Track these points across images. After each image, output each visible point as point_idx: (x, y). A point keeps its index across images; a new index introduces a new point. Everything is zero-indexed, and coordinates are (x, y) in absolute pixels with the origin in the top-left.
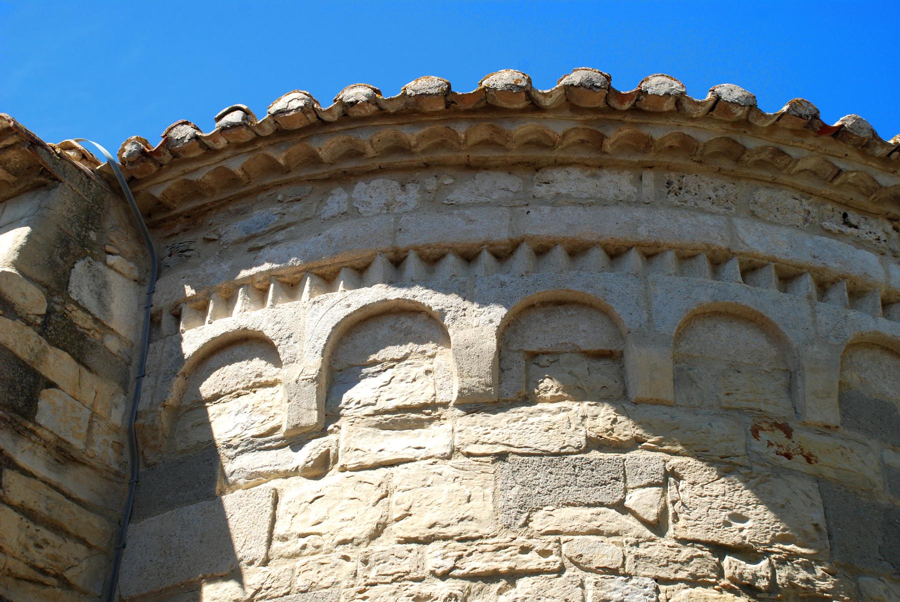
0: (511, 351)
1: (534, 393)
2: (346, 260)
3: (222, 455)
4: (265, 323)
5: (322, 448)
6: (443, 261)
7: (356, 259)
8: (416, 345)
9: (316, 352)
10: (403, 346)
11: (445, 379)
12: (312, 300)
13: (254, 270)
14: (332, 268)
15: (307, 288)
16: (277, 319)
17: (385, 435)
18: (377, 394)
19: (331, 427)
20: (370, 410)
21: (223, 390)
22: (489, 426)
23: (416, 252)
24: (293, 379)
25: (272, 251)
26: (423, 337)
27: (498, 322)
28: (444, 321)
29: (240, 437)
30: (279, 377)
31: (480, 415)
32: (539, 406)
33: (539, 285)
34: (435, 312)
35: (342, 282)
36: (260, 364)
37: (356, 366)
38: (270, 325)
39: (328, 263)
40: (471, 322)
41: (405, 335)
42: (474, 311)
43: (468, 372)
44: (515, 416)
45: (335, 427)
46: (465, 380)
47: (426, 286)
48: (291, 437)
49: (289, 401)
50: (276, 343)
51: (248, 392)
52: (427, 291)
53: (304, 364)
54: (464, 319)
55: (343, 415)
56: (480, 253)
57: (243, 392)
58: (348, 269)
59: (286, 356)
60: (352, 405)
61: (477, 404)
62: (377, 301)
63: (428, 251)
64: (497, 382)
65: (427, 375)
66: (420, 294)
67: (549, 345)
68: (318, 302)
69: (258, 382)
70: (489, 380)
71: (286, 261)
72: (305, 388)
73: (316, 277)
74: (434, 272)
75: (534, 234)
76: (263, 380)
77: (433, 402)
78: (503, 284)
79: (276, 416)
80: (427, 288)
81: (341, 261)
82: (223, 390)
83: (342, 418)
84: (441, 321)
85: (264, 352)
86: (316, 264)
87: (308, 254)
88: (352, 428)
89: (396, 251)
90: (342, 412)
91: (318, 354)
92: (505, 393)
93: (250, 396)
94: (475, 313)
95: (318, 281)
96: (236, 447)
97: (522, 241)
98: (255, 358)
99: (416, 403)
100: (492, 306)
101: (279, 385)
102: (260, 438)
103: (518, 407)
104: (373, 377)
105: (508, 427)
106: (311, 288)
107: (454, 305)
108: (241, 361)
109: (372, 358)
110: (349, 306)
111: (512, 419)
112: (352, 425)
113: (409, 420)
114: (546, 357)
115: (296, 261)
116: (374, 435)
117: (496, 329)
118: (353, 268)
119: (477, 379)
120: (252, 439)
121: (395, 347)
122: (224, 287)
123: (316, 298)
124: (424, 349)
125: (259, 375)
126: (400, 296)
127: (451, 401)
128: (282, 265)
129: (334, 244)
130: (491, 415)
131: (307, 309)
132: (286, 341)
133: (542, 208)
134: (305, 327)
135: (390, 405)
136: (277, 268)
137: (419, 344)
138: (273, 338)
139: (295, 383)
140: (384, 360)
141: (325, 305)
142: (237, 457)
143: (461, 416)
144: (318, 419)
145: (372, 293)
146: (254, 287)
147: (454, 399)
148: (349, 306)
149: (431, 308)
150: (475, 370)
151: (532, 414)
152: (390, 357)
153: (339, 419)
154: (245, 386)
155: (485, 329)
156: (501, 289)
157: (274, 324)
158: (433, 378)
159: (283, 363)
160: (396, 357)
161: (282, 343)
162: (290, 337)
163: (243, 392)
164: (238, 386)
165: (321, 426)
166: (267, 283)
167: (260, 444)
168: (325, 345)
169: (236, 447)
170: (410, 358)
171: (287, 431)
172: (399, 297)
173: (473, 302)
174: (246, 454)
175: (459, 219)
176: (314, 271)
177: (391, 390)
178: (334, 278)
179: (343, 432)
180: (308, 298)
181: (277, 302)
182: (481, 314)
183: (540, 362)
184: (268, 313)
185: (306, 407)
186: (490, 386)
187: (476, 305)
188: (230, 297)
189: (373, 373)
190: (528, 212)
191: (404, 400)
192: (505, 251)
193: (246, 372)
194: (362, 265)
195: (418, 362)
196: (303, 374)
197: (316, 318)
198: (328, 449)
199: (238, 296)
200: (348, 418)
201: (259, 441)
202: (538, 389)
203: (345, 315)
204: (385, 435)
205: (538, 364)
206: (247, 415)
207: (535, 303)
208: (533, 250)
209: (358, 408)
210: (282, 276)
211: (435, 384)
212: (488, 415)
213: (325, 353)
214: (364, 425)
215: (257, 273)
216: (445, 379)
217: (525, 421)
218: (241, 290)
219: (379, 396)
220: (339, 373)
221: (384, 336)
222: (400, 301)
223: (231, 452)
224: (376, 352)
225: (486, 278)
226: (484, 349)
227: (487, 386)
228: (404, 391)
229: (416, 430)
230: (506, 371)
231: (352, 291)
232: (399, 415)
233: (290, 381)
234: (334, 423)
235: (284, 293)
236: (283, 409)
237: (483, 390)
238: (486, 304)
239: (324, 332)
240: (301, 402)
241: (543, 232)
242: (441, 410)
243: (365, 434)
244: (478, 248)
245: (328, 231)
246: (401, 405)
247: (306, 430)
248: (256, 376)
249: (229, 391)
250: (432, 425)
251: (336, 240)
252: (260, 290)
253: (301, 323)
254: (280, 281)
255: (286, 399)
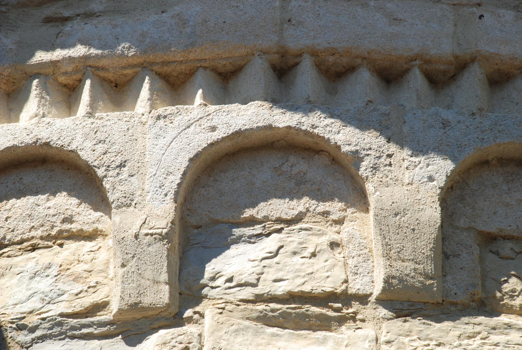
0: (457, 228)
1: (495, 297)
2: (207, 57)
3: (9, 340)
4: (79, 138)
5: (177, 344)
6: (352, 78)
7: (222, 58)
8: (314, 202)
9: (166, 195)
10: (295, 201)
11: (360, 259)
12: (155, 113)
13: (58, 54)
14: (183, 67)
15: (145, 92)
16: (100, 136)
17: (273, 335)
18: (258, 270)
19: (188, 313)
20: (247, 293)
21: (8, 237)
22: (431, 340)
23: (313, 58)
24: (130, 231)
25: (88, 27)
26: (324, 191)
27: (441, 180)
28: (358, 169)
29: (40, 314)
30: (100, 227)
31: (416, 322)
32: (504, 319)
33: (499, 132)
34: (346, 154)
35: (200, 91)
36: (69, 202)
37: (223, 223)
38: (88, 144)
39: (179, 57)
40: (401, 176)
41: (297, 184)
42: (403, 160)
43: (399, 252)
44: (470, 329)
45: (195, 313)
46: (394, 264)
47: (330, 113)
48: (125, 323)
49: (123, 266)
50: (100, 172)
51: (50, 244)
52: (333, 120)
53: (146, 210)
54: (389, 171)
55: (206, 297)
56: (407, 71)
57: (42, 243)
58: (208, 71)
59: (117, 195)
60: (220, 282)
61: (413, 304)
62: (258, 127)
63: (331, 59)
64: (440, 274)
65: (332, 249)
66: (322, 124)
67: (514, 227)
68: (165, 117)
69: (66, 231)
70: (430, 268)
71: (113, 47)
72: (150, 249)
73: (157, 77)
74: (336, 93)
75: (492, 51)
76: (74, 227)
77: (345, 293)
78: (445, 124)
79: (98, 287)
80: (332, 117)
81: (199, 57)
82: (8, 237)
83: (205, 301)
84: (353, 169)
85: (75, 184)
86: (160, 57)
87: (148, 40)
88: (222, 318)
89: (283, 53)
90: (205, 291)
91: (168, 198)
92: (453, 292)
93: (54, 252)
94: (406, 164)
95: (160, 84)
96: (33, 330)
97: (473, 60)
98: (61, 192)
99: (319, 290)
100: (432, 155)
101: (100, 239)
102: (74, 318)
103: (472, 316)
104: (250, 242)
105: (460, 345)
106: (152, 94)
107: (373, 147)
108: (36, 193)
109: (248, 213)
110: (213, 129)
111: (465, 333)
112: (221, 313)
113: (308, 316)
114: (509, 245)
115: (129, 48)
116: (256, 333)
117: (439, 191)
118: (214, 70)
119: (411, 265)
120: (59, 319)
121: (282, 201)
122: (6, 74)
123: (161, 110)
124: (327, 209)
125: (68, 220)
126: (293, 124)
127: (371, 294)
128: (106, 52)
129: (188, 30)
130: (434, 324)
131: (147, 126)
132: (117, 171)
133: (502, 11)
134: (147, 153)
135: (281, 289)
136: (97, 55)
137: (318, 200)
138: (95, 164)
139: (134, 239)
140: (266, 219)
141: (176, 123)
142: (35, 346)
143: (388, 320)
144: (170, 298)
145: (249, 113)
146: (56, 80)
147: (377, 289)
148: (213, 129)
149: (339, 147)
150: (409, 251)
151: (494, 329)
152: (275, 215)
153: (201, 302)
154: (45, 234)
155: (422, 188)
156: (443, 131)
157: (94, 142)
158: (342, 255)
159: (113, 206)
160: (284, 217)
161: (110, 173)
162: (122, 165)
163: (42, 243)
164: (33, 233)
165: (174, 310)
166: (78, 76)
167: (73, 328)
168: (179, 185)
169: (33, 330)
170: (306, 220)
171: (120, 311)
172: (291, 124)
173: (402, 148)
174: (49, 341)
175: (378, 15)
176: (156, 68)
177: (280, 266)
178: (184, 83)
179: (208, 321)
180: (148, 109)
181: (97, 109)
182: (416, 166)
183: (500, 251)
184: (84, 123)
185: (151, 278)
186: (431, 278)
187: (406, 152)
188: (13, 91)
189: (250, 237)
190: (481, 17)
191: (299, 283)
192: (444, 72)
193: (47, 212)
194: (229, 68)
195: (319, 228)
196: (146, 226)
197: (162, 142)
198: (186, 347)
199: (29, 92)
200: (215, 302)
201: (72, 324)
202: (500, 291)
203: (209, 142)
204: (273, 335)
205: (497, 253)
206: (50, 281)
207: (490, 158)
208: (487, 76)
209: (230, 288)
210: (103, 69)
211: (345, 264)
212: (431, 323)
213: (179, 196)
214: (240, 314)
215: (64, 59)
216: (360, 259)
217: (484, 339)
218: (35, 82)
219: (262, 274)
220: (196, 231)
221: (264, 182)
222: (292, 130)
223: (24, 337)
224: (254, 205)
225: (420, 111)
226: (422, 220)
227: (427, 277)
228: (298, 270)
229: (319, 333)
230: (451, 258)
231: (217, 107)
232: (293, 306)
233: (126, 234)
234: (192, 307)
235: (105, 96)
236: (110, 277)
237: (421, 282)
238: (422, 151)
239: (178, 165)
240: (143, 269)
241: (505, 51)
242: (356, 306)
243: (243, 330)
244: (406, 63)
245: (176, 8)
246: (297, 290)
247: (150, 313)
248: (64, 221)
249: (18, 238)
250: (343, 328)
251: (191, 23)
252: (65, 86)
253: (139, 146)
254: (100, 77)
255: (119, 261)
